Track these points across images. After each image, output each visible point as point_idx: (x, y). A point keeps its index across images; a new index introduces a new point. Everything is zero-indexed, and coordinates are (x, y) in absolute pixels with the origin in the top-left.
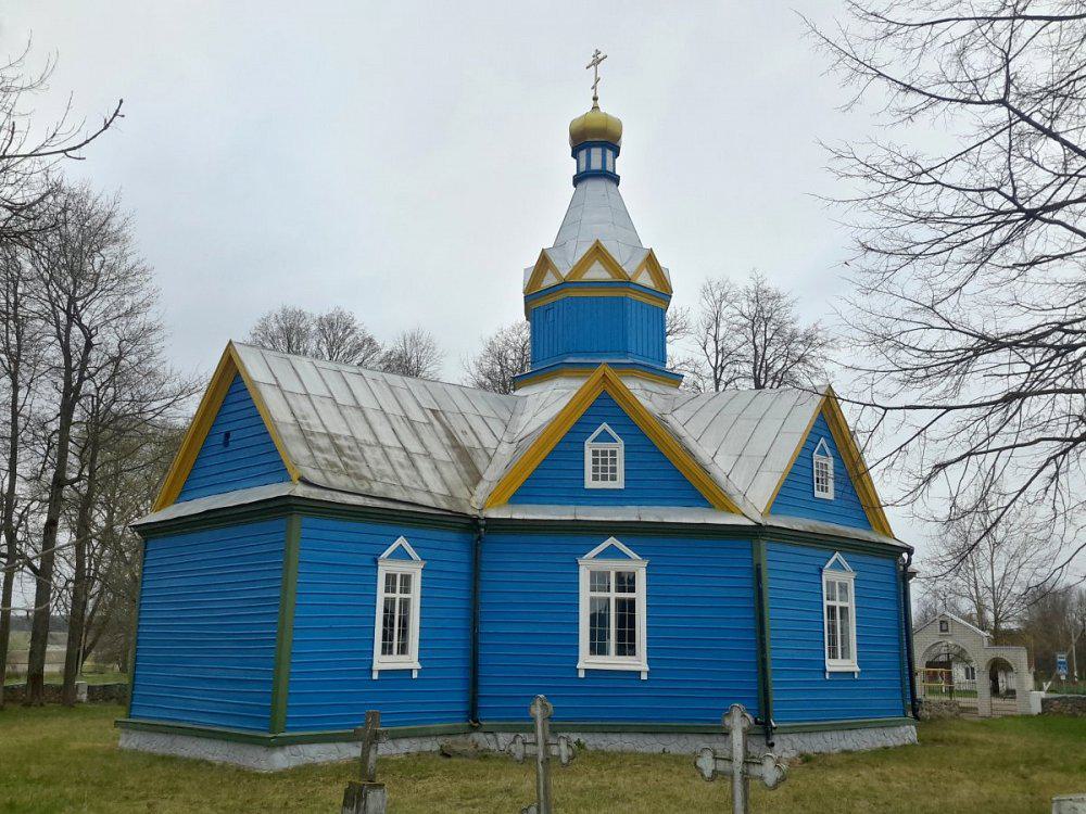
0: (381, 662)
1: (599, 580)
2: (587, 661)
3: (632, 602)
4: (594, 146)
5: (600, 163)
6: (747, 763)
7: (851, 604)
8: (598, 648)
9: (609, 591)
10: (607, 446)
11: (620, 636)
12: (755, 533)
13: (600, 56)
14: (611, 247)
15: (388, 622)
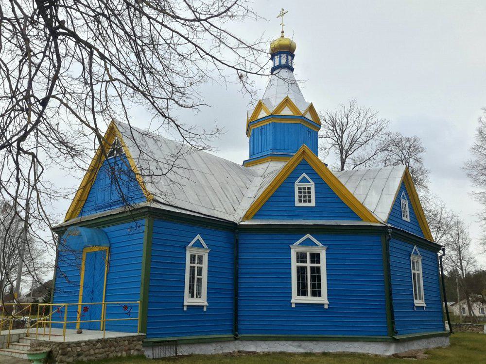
0: (188, 301)
1: (301, 257)
2: (296, 299)
3: (319, 269)
4: (284, 53)
7: (421, 272)
8: (302, 292)
9: (306, 263)
10: (306, 185)
11: (313, 286)
12: (380, 231)
13: (284, 12)
14: (292, 98)
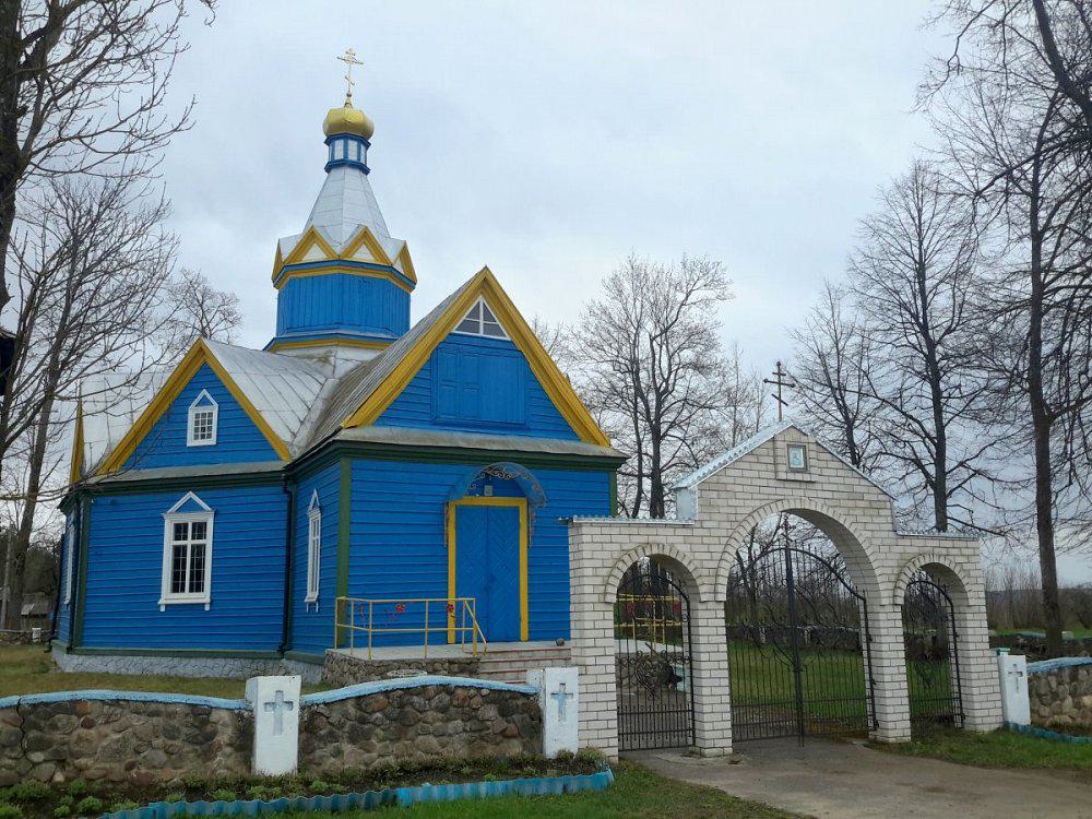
1: (180, 531)
2: (167, 597)
5: (350, 147)
8: (177, 587)
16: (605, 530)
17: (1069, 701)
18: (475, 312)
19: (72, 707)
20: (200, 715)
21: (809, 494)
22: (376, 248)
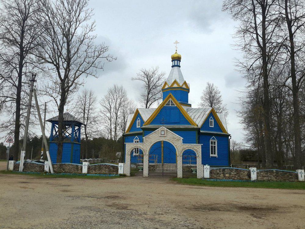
1: (212, 143)
2: (211, 155)
6: (53, 165)
14: (178, 81)
15: (212, 149)
16: (130, 145)
17: (222, 175)
18: (169, 102)
19: (65, 164)
20: (77, 166)
21: (165, 138)
22: (178, 84)
